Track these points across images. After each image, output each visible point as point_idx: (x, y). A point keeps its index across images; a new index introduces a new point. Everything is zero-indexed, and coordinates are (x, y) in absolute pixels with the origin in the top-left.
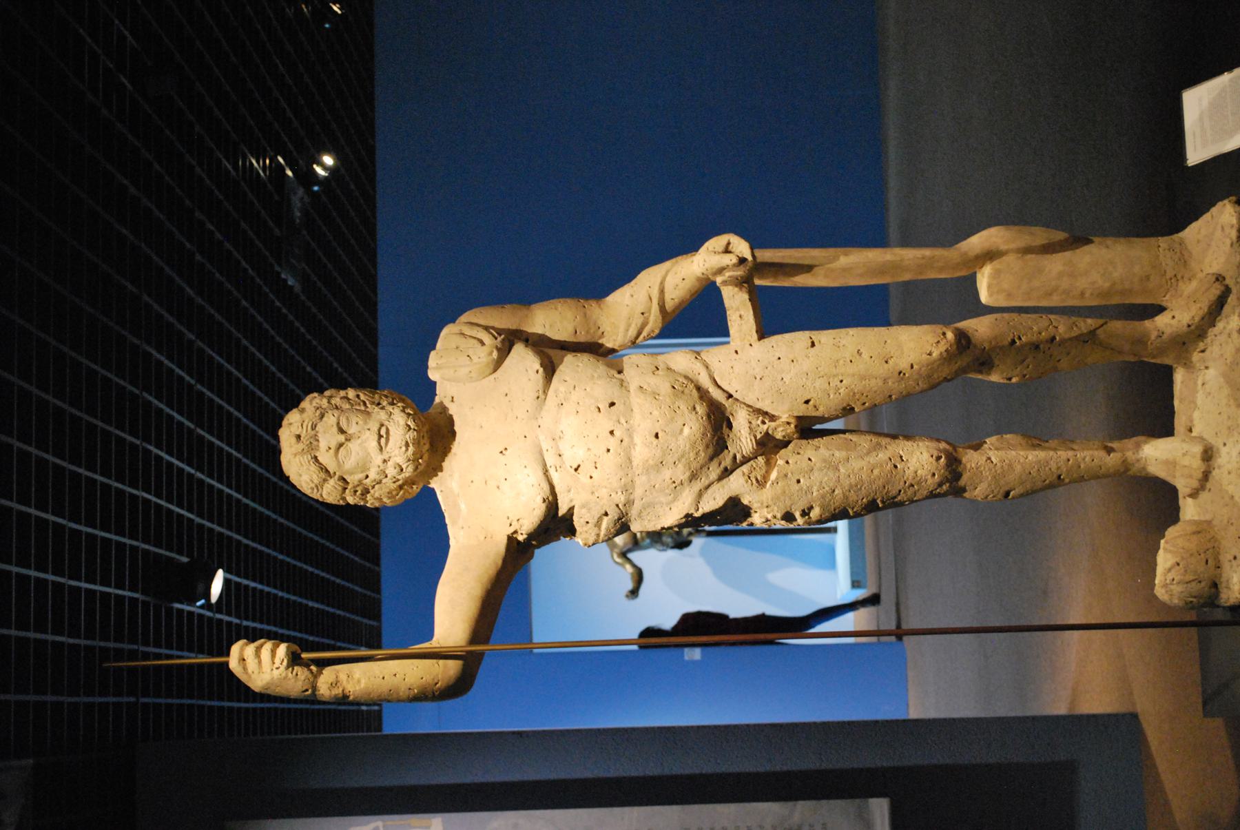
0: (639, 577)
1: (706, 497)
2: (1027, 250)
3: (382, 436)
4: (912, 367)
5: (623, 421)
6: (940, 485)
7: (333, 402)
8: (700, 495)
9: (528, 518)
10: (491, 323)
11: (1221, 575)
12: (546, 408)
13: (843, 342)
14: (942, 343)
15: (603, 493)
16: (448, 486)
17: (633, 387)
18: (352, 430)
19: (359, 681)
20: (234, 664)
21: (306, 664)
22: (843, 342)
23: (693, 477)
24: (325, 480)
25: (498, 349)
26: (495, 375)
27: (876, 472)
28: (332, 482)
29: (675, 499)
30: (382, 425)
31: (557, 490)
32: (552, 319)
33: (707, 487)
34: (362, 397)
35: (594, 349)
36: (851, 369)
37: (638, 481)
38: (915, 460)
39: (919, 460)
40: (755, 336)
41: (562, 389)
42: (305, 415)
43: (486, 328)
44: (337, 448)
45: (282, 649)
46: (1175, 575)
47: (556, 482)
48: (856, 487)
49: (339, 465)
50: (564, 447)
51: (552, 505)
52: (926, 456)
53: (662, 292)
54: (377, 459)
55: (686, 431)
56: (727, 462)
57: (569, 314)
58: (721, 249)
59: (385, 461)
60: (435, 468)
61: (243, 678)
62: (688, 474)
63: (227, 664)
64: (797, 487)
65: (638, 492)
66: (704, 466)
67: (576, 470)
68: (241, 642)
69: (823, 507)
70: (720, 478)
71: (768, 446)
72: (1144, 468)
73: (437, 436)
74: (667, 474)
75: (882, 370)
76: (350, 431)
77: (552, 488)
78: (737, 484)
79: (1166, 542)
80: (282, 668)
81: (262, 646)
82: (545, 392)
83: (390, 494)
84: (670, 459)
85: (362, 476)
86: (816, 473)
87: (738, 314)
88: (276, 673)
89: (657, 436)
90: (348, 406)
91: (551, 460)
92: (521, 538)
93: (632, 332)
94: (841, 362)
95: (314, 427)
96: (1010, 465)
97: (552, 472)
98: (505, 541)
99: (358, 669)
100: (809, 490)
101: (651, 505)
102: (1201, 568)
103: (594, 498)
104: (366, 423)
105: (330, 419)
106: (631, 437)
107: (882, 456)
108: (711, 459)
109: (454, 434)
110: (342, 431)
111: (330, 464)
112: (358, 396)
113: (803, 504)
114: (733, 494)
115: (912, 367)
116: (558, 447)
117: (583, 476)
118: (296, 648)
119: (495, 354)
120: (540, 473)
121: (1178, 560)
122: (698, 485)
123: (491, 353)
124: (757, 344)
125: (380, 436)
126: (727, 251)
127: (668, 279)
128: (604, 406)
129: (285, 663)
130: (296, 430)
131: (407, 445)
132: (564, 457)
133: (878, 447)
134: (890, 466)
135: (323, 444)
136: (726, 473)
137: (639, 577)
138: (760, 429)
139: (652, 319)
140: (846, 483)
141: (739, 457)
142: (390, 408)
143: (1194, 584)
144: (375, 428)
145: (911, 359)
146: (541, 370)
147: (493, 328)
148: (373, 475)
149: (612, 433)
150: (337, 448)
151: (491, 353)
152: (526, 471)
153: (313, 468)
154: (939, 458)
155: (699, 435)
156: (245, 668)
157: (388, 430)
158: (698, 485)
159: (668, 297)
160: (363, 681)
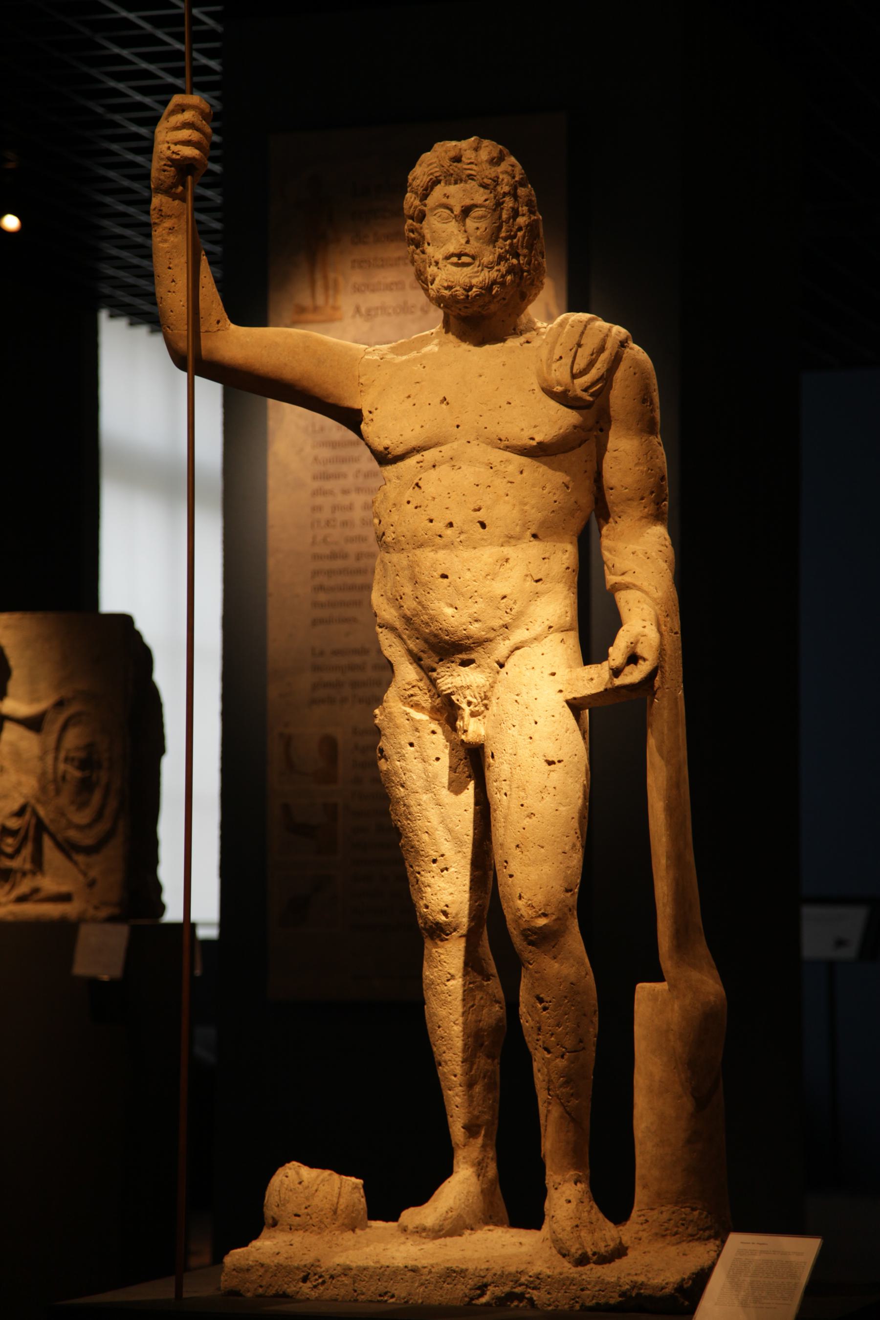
3: (459, 258)
4: (511, 876)
5: (462, 537)
7: (507, 199)
8: (393, 629)
11: (283, 1230)
12: (489, 448)
13: (548, 799)
14: (531, 912)
15: (395, 517)
17: (508, 551)
18: (470, 223)
19: (165, 241)
22: (548, 799)
23: (408, 620)
27: (425, 837)
29: (388, 599)
30: (474, 257)
31: (400, 464)
32: (627, 457)
33: (400, 637)
34: (520, 234)
37: (403, 556)
38: (443, 885)
40: (570, 696)
41: (512, 468)
42: (485, 166)
48: (408, 816)
49: (433, 209)
50: (444, 470)
52: (448, 899)
54: (439, 255)
55: (449, 611)
56: (427, 661)
57: (629, 480)
62: (408, 613)
67: (417, 484)
69: (388, 771)
70: (410, 652)
71: (447, 711)
74: (408, 589)
76: (468, 221)
78: (407, 673)
79: (500, 1237)
80: (169, 153)
81: (197, 129)
82: (507, 448)
84: (420, 592)
86: (420, 766)
87: (595, 676)
89: (444, 576)
90: (505, 216)
91: (429, 455)
94: (522, 794)
97: (418, 457)
100: (402, 758)
102: (291, 1208)
103: (390, 506)
104: (478, 239)
105: (480, 196)
106: (445, 547)
108: (426, 641)
109: (480, 342)
111: (431, 201)
112: (520, 229)
115: (511, 876)
116: (443, 463)
119: (558, 389)
120: (414, 443)
121: (305, 1184)
122: (398, 624)
123: (559, 384)
124: (561, 698)
125: (459, 256)
127: (638, 594)
128: (481, 515)
129: (174, 156)
130: (469, 156)
131: (449, 288)
132: (432, 471)
133: (457, 841)
134: (434, 855)
135: (452, 189)
136: (416, 659)
138: (461, 699)
141: (434, 674)
142: (503, 267)
144: (469, 249)
145: (517, 875)
146: (534, 443)
149: (451, 525)
151: (559, 384)
152: (418, 428)
154: (445, 914)
155: (445, 625)
158: (398, 624)
160: (165, 245)
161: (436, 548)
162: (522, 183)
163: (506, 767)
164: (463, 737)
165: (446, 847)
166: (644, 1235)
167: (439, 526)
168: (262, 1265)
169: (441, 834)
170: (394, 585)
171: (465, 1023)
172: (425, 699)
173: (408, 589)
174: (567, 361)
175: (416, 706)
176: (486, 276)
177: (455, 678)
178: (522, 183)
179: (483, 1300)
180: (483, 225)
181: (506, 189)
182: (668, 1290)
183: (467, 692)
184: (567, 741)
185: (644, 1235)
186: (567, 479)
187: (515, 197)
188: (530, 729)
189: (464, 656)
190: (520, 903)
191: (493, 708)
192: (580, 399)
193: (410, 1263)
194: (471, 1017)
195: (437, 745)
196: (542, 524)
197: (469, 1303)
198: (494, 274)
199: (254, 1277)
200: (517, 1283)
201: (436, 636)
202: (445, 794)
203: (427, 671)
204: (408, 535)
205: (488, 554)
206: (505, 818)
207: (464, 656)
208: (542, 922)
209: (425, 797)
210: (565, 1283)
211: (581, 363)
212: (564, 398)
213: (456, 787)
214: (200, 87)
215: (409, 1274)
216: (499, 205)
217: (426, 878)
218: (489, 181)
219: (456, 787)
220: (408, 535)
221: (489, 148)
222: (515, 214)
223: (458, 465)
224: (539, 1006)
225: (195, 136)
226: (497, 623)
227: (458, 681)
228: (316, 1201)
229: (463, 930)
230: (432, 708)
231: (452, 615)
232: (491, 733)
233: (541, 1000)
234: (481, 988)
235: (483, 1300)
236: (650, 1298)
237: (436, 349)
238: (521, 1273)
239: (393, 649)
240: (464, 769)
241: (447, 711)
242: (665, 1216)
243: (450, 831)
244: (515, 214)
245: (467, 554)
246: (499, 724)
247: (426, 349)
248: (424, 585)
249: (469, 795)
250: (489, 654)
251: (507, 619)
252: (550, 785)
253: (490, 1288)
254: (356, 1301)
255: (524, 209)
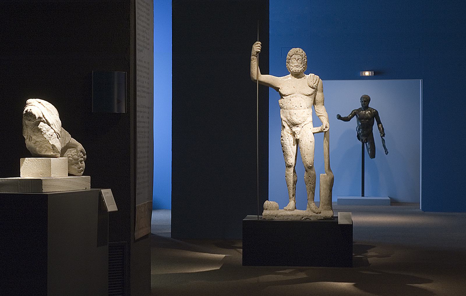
0: (346, 119)
1: (285, 122)
2: (305, 167)
5: (298, 108)
6: (287, 164)
8: (285, 121)
9: (282, 91)
10: (319, 85)
13: (311, 147)
16: (289, 77)
17: (304, 110)
20: (257, 42)
21: (257, 54)
23: (288, 120)
24: (290, 56)
25: (312, 87)
26: (308, 86)
27: (289, 152)
28: (290, 57)
31: (287, 96)
33: (287, 122)
34: (305, 62)
35: (314, 103)
36: (306, 148)
39: (291, 160)
43: (317, 84)
44: (296, 58)
45: (260, 50)
46: (339, 285)
47: (288, 96)
49: (292, 59)
51: (284, 96)
52: (292, 162)
53: (322, 116)
54: (293, 66)
55: (296, 119)
58: (327, 126)
59: (293, 67)
60: (292, 75)
61: (255, 44)
63: (257, 41)
64: (287, 138)
65: (286, 111)
66: (290, 122)
68: (261, 43)
69: (283, 143)
70: (288, 125)
71: (294, 134)
72: (290, 202)
73: (297, 75)
75: (305, 154)
77: (287, 96)
78: (287, 128)
82: (304, 95)
83: (288, 67)
85: (291, 62)
86: (289, 142)
88: (255, 49)
92: (279, 90)
93: (316, 110)
95: (299, 54)
96: (290, 177)
97: (290, 96)
98: (279, 87)
99: (256, 63)
101: (284, 113)
106: (295, 109)
107: (292, 154)
110: (298, 59)
113: (283, 139)
114: (285, 127)
117: (289, 101)
118: (260, 52)
124: (312, 132)
126: (326, 127)
128: (301, 105)
131: (295, 71)
134: (290, 155)
135: (296, 56)
136: (289, 126)
137: (346, 119)
139: (318, 114)
140: (287, 147)
141: (292, 128)
142: (303, 67)
143: (267, 206)
147: (318, 85)
148: (291, 64)
150: (296, 58)
151: (312, 85)
153: (292, 54)
154: (292, 164)
156: (256, 44)
157: (298, 67)
159: (321, 117)
161: (294, 110)
162: (306, 55)
163: (304, 142)
164: (297, 138)
165: (292, 154)
166: (322, 210)
167: (294, 106)
168: (269, 215)
169: (291, 152)
170: (286, 115)
171: (293, 180)
172: (290, 132)
173: (289, 116)
174: (312, 82)
175: (288, 133)
176: (301, 69)
177: (295, 129)
178: (306, 55)
179: (303, 219)
180: (300, 61)
181: (304, 56)
182: (330, 217)
183: (297, 131)
184: (312, 138)
185: (322, 210)
186: (312, 99)
187: (305, 57)
188: (308, 137)
189: (297, 126)
190: (307, 163)
191: (301, 133)
192: (314, 87)
193: (292, 214)
194: (294, 179)
195: (291, 139)
196: (309, 106)
197: (301, 220)
198: (302, 69)
199: (268, 217)
200: (308, 216)
201: (293, 123)
202: (292, 146)
203: (291, 128)
204: (289, 107)
205: (302, 111)
206: (304, 150)
207: (297, 126)
208: (311, 165)
209: (289, 147)
210: (315, 216)
211: (314, 82)
212: (312, 88)
213: (294, 145)
214: (367, 114)
215: (292, 216)
216: (303, 58)
217: (288, 158)
218: (302, 55)
219: (294, 145)
220: (289, 107)
221: (301, 50)
222: (305, 59)
223: (296, 97)
224: (310, 178)
225: (260, 48)
226: (303, 121)
227: (296, 130)
228: (273, 206)
229: (294, 166)
230: (291, 133)
231: (296, 120)
232: (301, 137)
233: (310, 177)
234: (295, 175)
235: (303, 219)
236: (328, 218)
237: (291, 79)
238: (309, 215)
239: (285, 124)
240: (295, 142)
241: (294, 134)
242: (325, 207)
243: (293, 152)
244: (305, 59)
245: (299, 111)
246: (302, 136)
247: (289, 79)
248: (292, 115)
249: (296, 146)
250: (301, 125)
251: (304, 120)
252: (311, 145)
253: (304, 217)
254: (283, 220)
255: (306, 59)
